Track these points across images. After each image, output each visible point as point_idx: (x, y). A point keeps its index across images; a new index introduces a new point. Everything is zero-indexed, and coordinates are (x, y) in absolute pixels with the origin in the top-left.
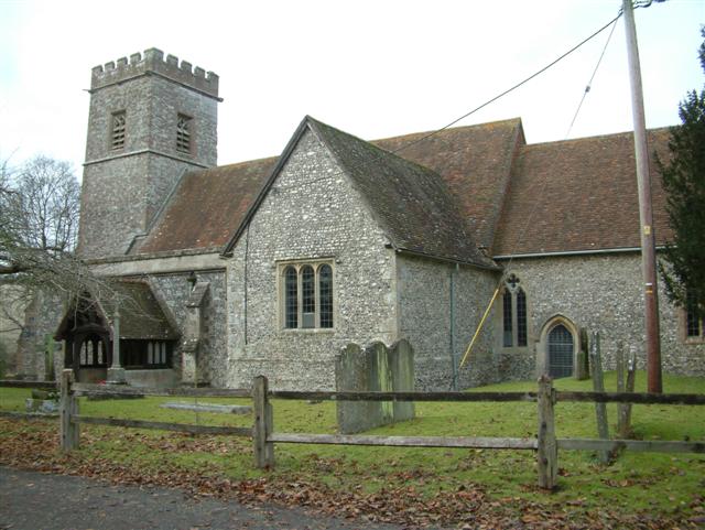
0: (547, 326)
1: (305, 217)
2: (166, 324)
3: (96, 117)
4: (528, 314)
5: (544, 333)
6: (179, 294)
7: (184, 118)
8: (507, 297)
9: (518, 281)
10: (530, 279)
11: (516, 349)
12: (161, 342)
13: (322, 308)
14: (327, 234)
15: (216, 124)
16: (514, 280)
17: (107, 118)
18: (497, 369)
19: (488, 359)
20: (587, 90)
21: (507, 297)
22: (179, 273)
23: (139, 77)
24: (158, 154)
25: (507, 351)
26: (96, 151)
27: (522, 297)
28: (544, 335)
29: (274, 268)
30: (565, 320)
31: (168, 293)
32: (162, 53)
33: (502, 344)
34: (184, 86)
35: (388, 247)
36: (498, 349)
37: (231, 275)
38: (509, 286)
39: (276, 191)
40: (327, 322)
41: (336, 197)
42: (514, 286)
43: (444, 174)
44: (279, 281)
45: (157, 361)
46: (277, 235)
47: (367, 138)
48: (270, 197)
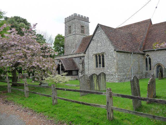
0: (156, 66)
1: (99, 45)
2: (76, 67)
3: (66, 28)
4: (151, 63)
5: (155, 67)
6: (79, 61)
7: (82, 27)
8: (146, 59)
9: (149, 56)
10: (152, 55)
11: (148, 71)
12: (75, 70)
13: (102, 63)
14: (103, 48)
15: (89, 27)
16: (148, 56)
17: (68, 28)
18: (144, 75)
19: (142, 73)
20: (156, 8)
21: (146, 59)
22: (78, 57)
23: (73, 19)
24: (77, 34)
25: (147, 71)
26: (66, 35)
27: (150, 59)
28: (155, 68)
29: (93, 55)
30: (161, 64)
31: (77, 61)
32: (77, 14)
33: (145, 70)
34: (82, 20)
35: (115, 50)
36: (144, 71)
37: (86, 57)
38: (147, 57)
39: (93, 40)
40: (103, 66)
41: (104, 40)
42: (148, 57)
43: (133, 33)
44: (94, 58)
45: (75, 74)
46: (93, 49)
47: (115, 28)
48: (92, 41)
